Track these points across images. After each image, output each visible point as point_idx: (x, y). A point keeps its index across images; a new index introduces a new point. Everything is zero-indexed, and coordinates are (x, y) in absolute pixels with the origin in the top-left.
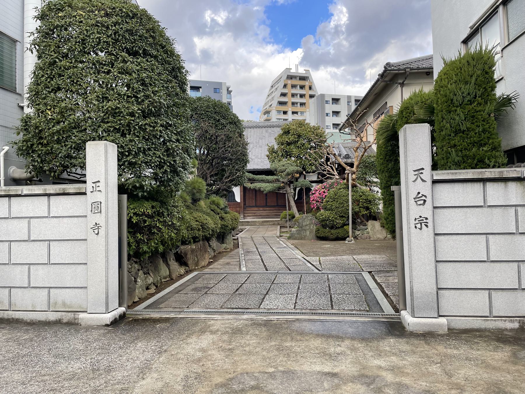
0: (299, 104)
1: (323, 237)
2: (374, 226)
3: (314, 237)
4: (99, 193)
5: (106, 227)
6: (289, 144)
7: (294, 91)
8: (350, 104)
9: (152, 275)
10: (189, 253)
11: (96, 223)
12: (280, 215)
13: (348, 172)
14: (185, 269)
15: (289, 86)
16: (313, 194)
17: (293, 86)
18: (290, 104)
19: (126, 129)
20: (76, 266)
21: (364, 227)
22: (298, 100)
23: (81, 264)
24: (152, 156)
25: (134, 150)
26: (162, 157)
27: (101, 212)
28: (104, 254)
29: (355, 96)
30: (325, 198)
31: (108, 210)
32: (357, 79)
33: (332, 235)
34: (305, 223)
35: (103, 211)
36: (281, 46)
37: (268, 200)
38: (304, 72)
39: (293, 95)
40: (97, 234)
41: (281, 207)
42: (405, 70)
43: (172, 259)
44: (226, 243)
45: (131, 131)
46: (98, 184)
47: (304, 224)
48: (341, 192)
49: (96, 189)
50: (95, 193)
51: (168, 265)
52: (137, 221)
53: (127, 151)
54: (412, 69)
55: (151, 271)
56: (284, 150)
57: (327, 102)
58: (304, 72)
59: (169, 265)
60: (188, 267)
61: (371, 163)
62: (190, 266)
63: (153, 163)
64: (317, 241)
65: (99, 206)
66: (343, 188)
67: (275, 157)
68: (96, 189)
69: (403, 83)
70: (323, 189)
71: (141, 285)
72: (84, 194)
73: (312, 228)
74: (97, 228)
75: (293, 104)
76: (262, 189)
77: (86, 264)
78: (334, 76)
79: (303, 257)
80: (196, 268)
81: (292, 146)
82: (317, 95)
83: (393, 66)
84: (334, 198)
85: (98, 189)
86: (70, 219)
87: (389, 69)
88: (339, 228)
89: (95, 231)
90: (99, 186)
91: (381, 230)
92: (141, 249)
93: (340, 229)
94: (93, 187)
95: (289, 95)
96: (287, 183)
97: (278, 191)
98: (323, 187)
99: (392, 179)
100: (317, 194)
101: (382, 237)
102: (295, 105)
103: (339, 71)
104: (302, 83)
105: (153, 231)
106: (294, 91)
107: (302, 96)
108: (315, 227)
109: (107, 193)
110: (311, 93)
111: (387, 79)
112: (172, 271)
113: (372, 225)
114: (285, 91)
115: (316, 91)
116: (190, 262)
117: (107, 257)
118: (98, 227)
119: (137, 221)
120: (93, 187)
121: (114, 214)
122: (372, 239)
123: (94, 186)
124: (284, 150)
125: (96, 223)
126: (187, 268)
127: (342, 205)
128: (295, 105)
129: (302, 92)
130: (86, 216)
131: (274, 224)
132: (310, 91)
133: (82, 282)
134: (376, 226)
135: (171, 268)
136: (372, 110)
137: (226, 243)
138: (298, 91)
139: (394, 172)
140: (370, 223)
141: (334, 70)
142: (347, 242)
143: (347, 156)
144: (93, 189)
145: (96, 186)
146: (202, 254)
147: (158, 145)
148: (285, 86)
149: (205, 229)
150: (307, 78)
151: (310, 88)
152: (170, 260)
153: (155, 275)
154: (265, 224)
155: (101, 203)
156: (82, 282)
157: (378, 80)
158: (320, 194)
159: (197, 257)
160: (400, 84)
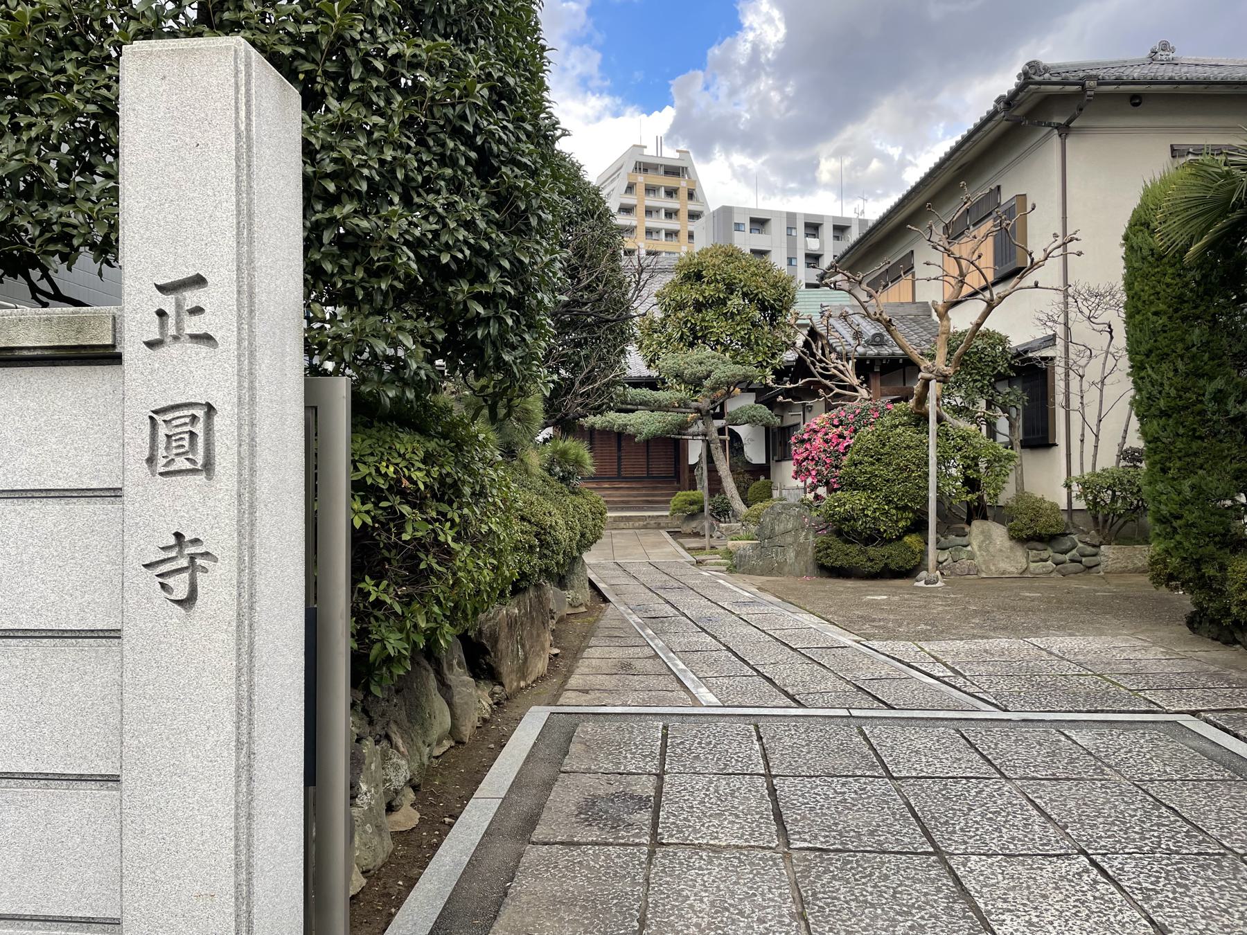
0: (663, 232)
1: (841, 567)
2: (987, 536)
3: (811, 567)
4: (203, 349)
5: (240, 559)
6: (699, 307)
7: (651, 201)
8: (794, 234)
9: (400, 743)
10: (503, 634)
11: (178, 536)
12: (668, 502)
13: (928, 375)
14: (492, 695)
15: (640, 189)
16: (803, 441)
17: (651, 190)
18: (641, 232)
19: (325, 73)
20: (58, 790)
21: (959, 540)
22: (661, 223)
23: (81, 778)
24: (441, 219)
25: (366, 172)
26: (482, 225)
27: (208, 467)
28: (230, 727)
29: (805, 215)
30: (844, 454)
31: (252, 455)
32: (792, 185)
33: (869, 564)
34: (782, 526)
35: (225, 460)
36: (619, 101)
37: (624, 462)
38: (677, 155)
39: (649, 212)
40: (188, 602)
41: (659, 482)
42: (1083, 85)
43: (455, 662)
44: (573, 587)
45: (348, 79)
46: (192, 297)
47: (779, 528)
48: (900, 435)
49: (179, 327)
50: (171, 351)
51: (445, 687)
52: (369, 521)
53: (332, 176)
54: (1102, 82)
55: (394, 727)
56: (685, 323)
57: (738, 227)
58: (677, 155)
59: (449, 687)
60: (501, 684)
61: (975, 353)
62: (506, 681)
63: (448, 247)
64: (819, 579)
65: (199, 429)
66: (903, 425)
67: (660, 343)
68: (179, 327)
69: (1067, 125)
70: (837, 427)
71: (370, 809)
72: (108, 356)
73: (802, 540)
74: (184, 562)
75: (649, 232)
76: (631, 430)
77: (115, 779)
78: (743, 175)
79: (855, 641)
80: (522, 684)
81: (710, 314)
82: (706, 213)
83: (1046, 70)
84: (878, 453)
85: (194, 325)
86: (22, 506)
87: (1037, 78)
88: (890, 541)
89: (170, 581)
90: (197, 311)
91: (1011, 548)
92: (377, 647)
93: (894, 545)
94: (161, 314)
95: (640, 211)
96: (708, 411)
97: (679, 434)
98: (836, 422)
99: (1202, 382)
100: (818, 442)
101: (1012, 569)
102: (654, 236)
103: (753, 164)
104: (671, 182)
105: (423, 566)
106: (651, 201)
107: (670, 214)
108: (811, 538)
109: (248, 352)
110: (692, 206)
111: (1018, 112)
112: (459, 712)
113: (982, 532)
114: (630, 200)
115: (704, 203)
116: (507, 668)
117: (245, 746)
118: (192, 558)
119: (369, 521)
120: (161, 314)
121: (283, 481)
122: (984, 575)
123: (170, 309)
124: (685, 323)
125: (178, 536)
126: (497, 689)
127: (905, 475)
128: (654, 236)
129: (672, 204)
130: (115, 493)
131: (645, 527)
132: (690, 202)
133: (89, 890)
134: (994, 536)
135: (457, 699)
136: (1201, 121)
137: (573, 587)
138: (662, 201)
139: (1210, 359)
140: (977, 525)
141: (740, 159)
142: (922, 584)
143: (878, 339)
144: (163, 326)
145: (179, 306)
146: (535, 633)
147: (464, 172)
148: (630, 188)
149: (548, 546)
150: (684, 169)
151: (691, 195)
152: (451, 667)
153: (410, 742)
154: (622, 525)
155: (210, 409)
156: (89, 890)
157: (991, 116)
158: (826, 441)
159: (523, 646)
160: (1058, 127)
